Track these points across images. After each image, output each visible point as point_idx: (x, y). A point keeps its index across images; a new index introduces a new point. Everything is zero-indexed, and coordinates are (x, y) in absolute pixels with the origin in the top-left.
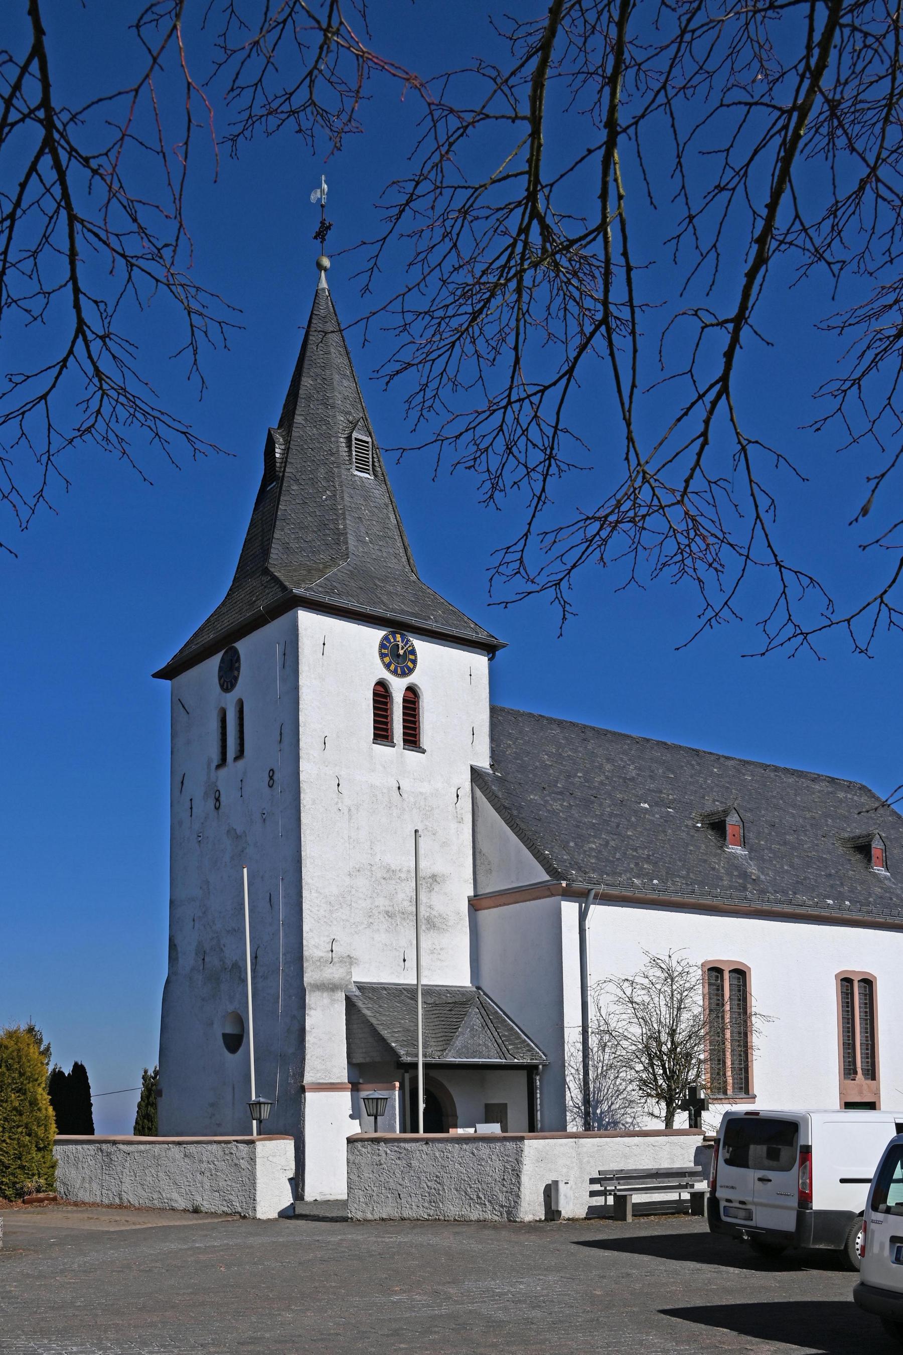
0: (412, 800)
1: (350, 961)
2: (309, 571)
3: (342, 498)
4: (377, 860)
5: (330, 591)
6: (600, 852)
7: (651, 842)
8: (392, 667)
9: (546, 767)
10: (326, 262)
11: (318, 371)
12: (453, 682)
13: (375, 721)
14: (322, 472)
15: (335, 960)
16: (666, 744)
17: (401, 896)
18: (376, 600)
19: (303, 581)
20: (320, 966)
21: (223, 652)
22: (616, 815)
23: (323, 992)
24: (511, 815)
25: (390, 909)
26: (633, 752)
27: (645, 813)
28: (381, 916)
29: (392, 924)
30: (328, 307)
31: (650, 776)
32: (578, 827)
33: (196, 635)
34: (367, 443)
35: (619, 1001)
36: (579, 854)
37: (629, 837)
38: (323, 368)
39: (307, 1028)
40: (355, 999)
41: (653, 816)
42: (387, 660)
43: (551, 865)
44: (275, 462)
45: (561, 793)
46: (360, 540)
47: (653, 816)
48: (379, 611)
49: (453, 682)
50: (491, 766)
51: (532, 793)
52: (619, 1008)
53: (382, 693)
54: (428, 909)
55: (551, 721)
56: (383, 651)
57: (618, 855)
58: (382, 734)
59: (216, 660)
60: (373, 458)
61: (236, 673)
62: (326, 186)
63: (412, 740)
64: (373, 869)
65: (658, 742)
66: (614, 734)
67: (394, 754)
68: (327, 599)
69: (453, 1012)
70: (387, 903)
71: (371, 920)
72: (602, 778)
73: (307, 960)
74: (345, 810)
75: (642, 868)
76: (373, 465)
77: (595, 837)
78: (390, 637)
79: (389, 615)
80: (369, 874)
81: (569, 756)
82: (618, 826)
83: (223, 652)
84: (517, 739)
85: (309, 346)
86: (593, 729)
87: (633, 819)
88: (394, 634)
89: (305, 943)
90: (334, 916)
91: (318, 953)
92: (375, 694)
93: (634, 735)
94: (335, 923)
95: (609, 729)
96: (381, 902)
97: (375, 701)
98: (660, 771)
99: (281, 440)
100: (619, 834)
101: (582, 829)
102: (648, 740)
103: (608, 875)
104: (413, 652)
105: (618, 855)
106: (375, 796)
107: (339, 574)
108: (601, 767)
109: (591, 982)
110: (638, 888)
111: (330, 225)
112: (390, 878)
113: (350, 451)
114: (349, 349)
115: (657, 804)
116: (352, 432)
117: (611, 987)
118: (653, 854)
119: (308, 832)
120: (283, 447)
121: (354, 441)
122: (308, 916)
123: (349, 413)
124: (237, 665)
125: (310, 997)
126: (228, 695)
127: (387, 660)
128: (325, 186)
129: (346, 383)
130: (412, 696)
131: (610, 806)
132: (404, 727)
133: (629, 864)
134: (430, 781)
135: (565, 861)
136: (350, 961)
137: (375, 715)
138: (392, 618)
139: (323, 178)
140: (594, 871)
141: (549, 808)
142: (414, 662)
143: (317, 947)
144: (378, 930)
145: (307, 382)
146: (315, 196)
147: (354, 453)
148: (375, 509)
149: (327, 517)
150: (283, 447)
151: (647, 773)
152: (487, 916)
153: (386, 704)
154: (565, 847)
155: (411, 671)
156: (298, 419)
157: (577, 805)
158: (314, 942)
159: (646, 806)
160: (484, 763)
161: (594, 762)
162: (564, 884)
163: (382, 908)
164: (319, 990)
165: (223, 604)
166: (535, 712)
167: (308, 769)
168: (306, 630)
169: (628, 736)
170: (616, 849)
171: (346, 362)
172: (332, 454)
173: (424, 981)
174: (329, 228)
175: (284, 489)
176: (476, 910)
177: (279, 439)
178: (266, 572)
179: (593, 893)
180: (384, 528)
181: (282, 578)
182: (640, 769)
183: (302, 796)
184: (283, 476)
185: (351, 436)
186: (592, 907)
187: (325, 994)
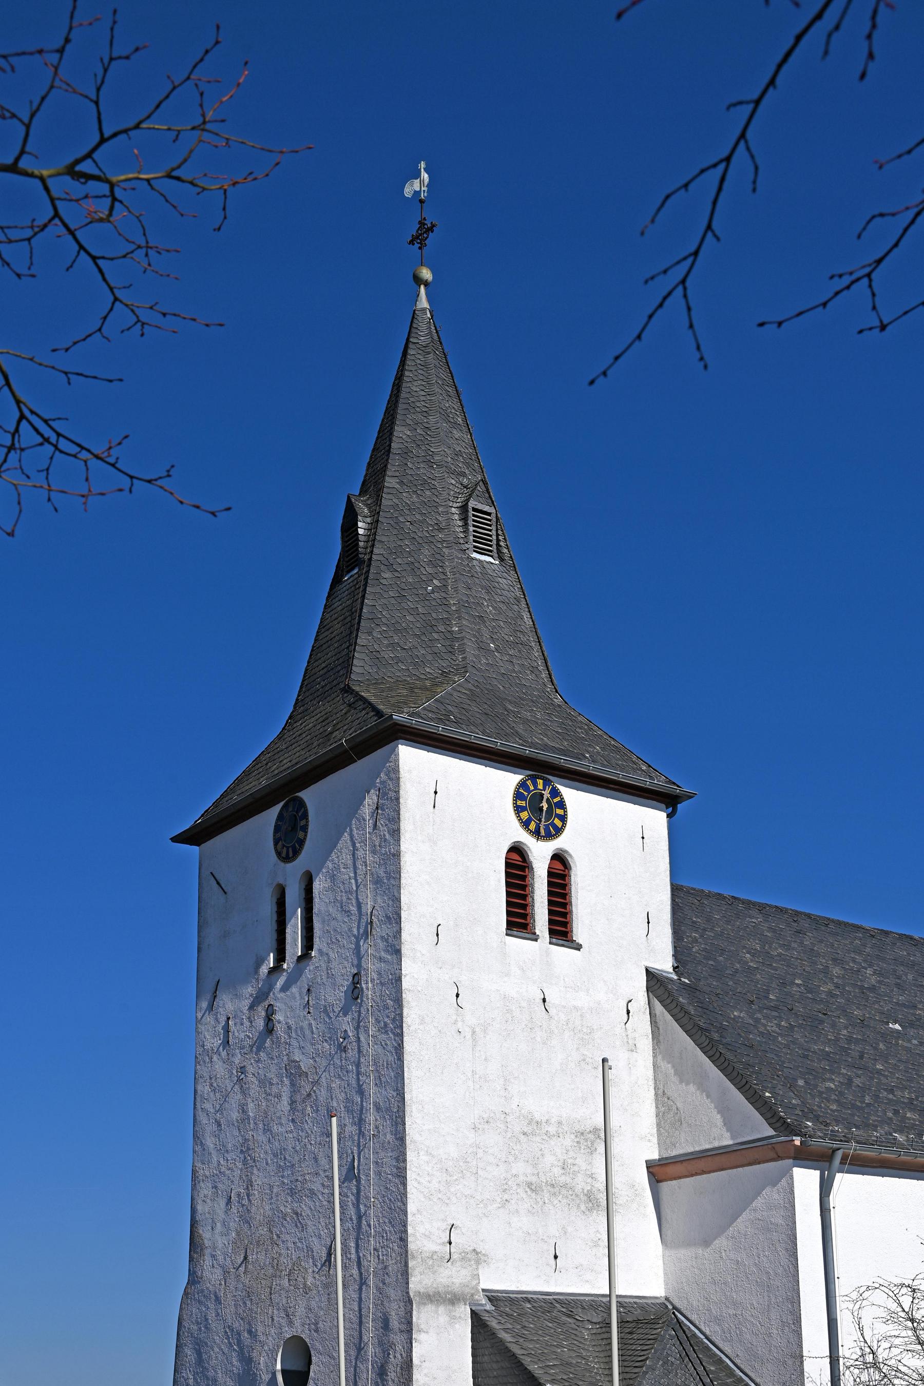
0: (563, 1017)
1: (477, 1257)
2: (411, 690)
3: (456, 590)
4: (514, 1107)
5: (444, 719)
6: (841, 1094)
7: (911, 1080)
8: (532, 826)
9: (750, 971)
10: (426, 274)
11: (419, 417)
12: (619, 849)
13: (509, 904)
14: (426, 553)
15: (454, 1256)
16: (911, 938)
17: (549, 1159)
18: (509, 731)
19: (405, 703)
20: (433, 1266)
21: (282, 804)
22: (857, 1041)
23: (437, 1306)
24: (711, 1040)
25: (534, 1179)
26: (868, 950)
27: (898, 1038)
28: (520, 1190)
29: (537, 1203)
30: (430, 332)
31: (897, 985)
32: (806, 1057)
33: (239, 781)
34: (489, 514)
35: (891, 1317)
36: (813, 1097)
37: (879, 1072)
38: (426, 414)
39: (415, 1360)
40: (486, 1317)
41: (909, 1041)
42: (525, 815)
43: (775, 1113)
44: (358, 540)
45: (776, 1008)
46: (482, 648)
47: (909, 1041)
48: (514, 746)
49: (619, 849)
50: (675, 968)
51: (735, 1008)
52: (892, 1329)
53: (517, 865)
54: (589, 1180)
55: (749, 904)
56: (519, 803)
57: (867, 1099)
58: (518, 921)
59: (273, 813)
60: (498, 535)
61: (301, 835)
62: (426, 176)
63: (561, 930)
64: (509, 1119)
65: (901, 935)
66: (839, 923)
67: (539, 949)
68: (441, 729)
69: (635, 1336)
70: (530, 1170)
71: (506, 1197)
72: (831, 986)
73: (413, 1257)
74: (467, 1032)
75: (904, 1117)
76: (498, 545)
77: (832, 1072)
78: (529, 783)
79: (527, 751)
80: (502, 1126)
81: (780, 955)
82: (861, 1057)
83: (282, 804)
84: (705, 930)
85: (404, 385)
86: (809, 916)
87: (881, 1046)
88: (534, 779)
89: (410, 1230)
90: (452, 1190)
91: (429, 1246)
92: (508, 865)
93: (867, 925)
94: (454, 1199)
95: (832, 917)
96: (521, 1168)
97: (508, 875)
98: (910, 977)
99: (366, 511)
100: (865, 1068)
101: (813, 1061)
102: (886, 933)
103: (857, 1127)
104: (562, 805)
105: (867, 1099)
106: (509, 1011)
107: (455, 694)
108: (826, 970)
109: (842, 1288)
110: (901, 1146)
111: (433, 226)
112: (533, 1134)
113: (466, 525)
114: (460, 389)
115: (912, 1025)
116: (468, 500)
117: (879, 1297)
118: (917, 1097)
119: (414, 1064)
120: (369, 520)
121: (471, 512)
122: (414, 1191)
123: (463, 475)
124: (303, 823)
125: (419, 1312)
126: (289, 866)
127: (525, 815)
128: (425, 176)
129: (457, 434)
130: (560, 869)
131: (846, 1028)
132: (551, 912)
133: (885, 1112)
134: (588, 991)
135: (794, 1107)
136: (477, 1257)
137: (509, 894)
138: (533, 756)
139: (423, 165)
140: (837, 1122)
141: (762, 1029)
142: (563, 819)
143: (427, 1236)
144: (517, 1211)
145: (401, 432)
146: (409, 190)
147: (471, 529)
148: (501, 605)
149: (434, 615)
150: (369, 520)
151: (891, 980)
152: (666, 1187)
153: (524, 878)
154: (792, 1086)
155: (559, 831)
156: (390, 482)
157: (800, 1026)
158: (424, 1228)
159: (897, 1027)
160: (665, 964)
161: (815, 963)
162: (797, 1141)
163: (522, 1178)
164: (432, 1301)
165: (280, 737)
166: (726, 893)
167: (412, 971)
168: (410, 771)
169: (858, 928)
170: (864, 1089)
171: (457, 406)
172: (440, 530)
173: (622, 1289)
174: (431, 229)
175: (371, 576)
176: (658, 1181)
177: (362, 508)
178: (348, 690)
179: (839, 1155)
180: (515, 631)
181: (373, 700)
182: (880, 974)
183: (405, 1012)
184: (370, 559)
185: (467, 504)
186: (839, 1176)
187: (441, 1309)
